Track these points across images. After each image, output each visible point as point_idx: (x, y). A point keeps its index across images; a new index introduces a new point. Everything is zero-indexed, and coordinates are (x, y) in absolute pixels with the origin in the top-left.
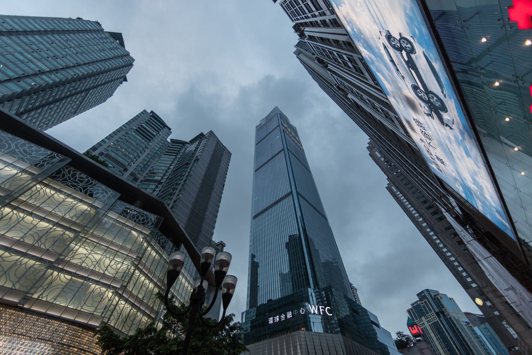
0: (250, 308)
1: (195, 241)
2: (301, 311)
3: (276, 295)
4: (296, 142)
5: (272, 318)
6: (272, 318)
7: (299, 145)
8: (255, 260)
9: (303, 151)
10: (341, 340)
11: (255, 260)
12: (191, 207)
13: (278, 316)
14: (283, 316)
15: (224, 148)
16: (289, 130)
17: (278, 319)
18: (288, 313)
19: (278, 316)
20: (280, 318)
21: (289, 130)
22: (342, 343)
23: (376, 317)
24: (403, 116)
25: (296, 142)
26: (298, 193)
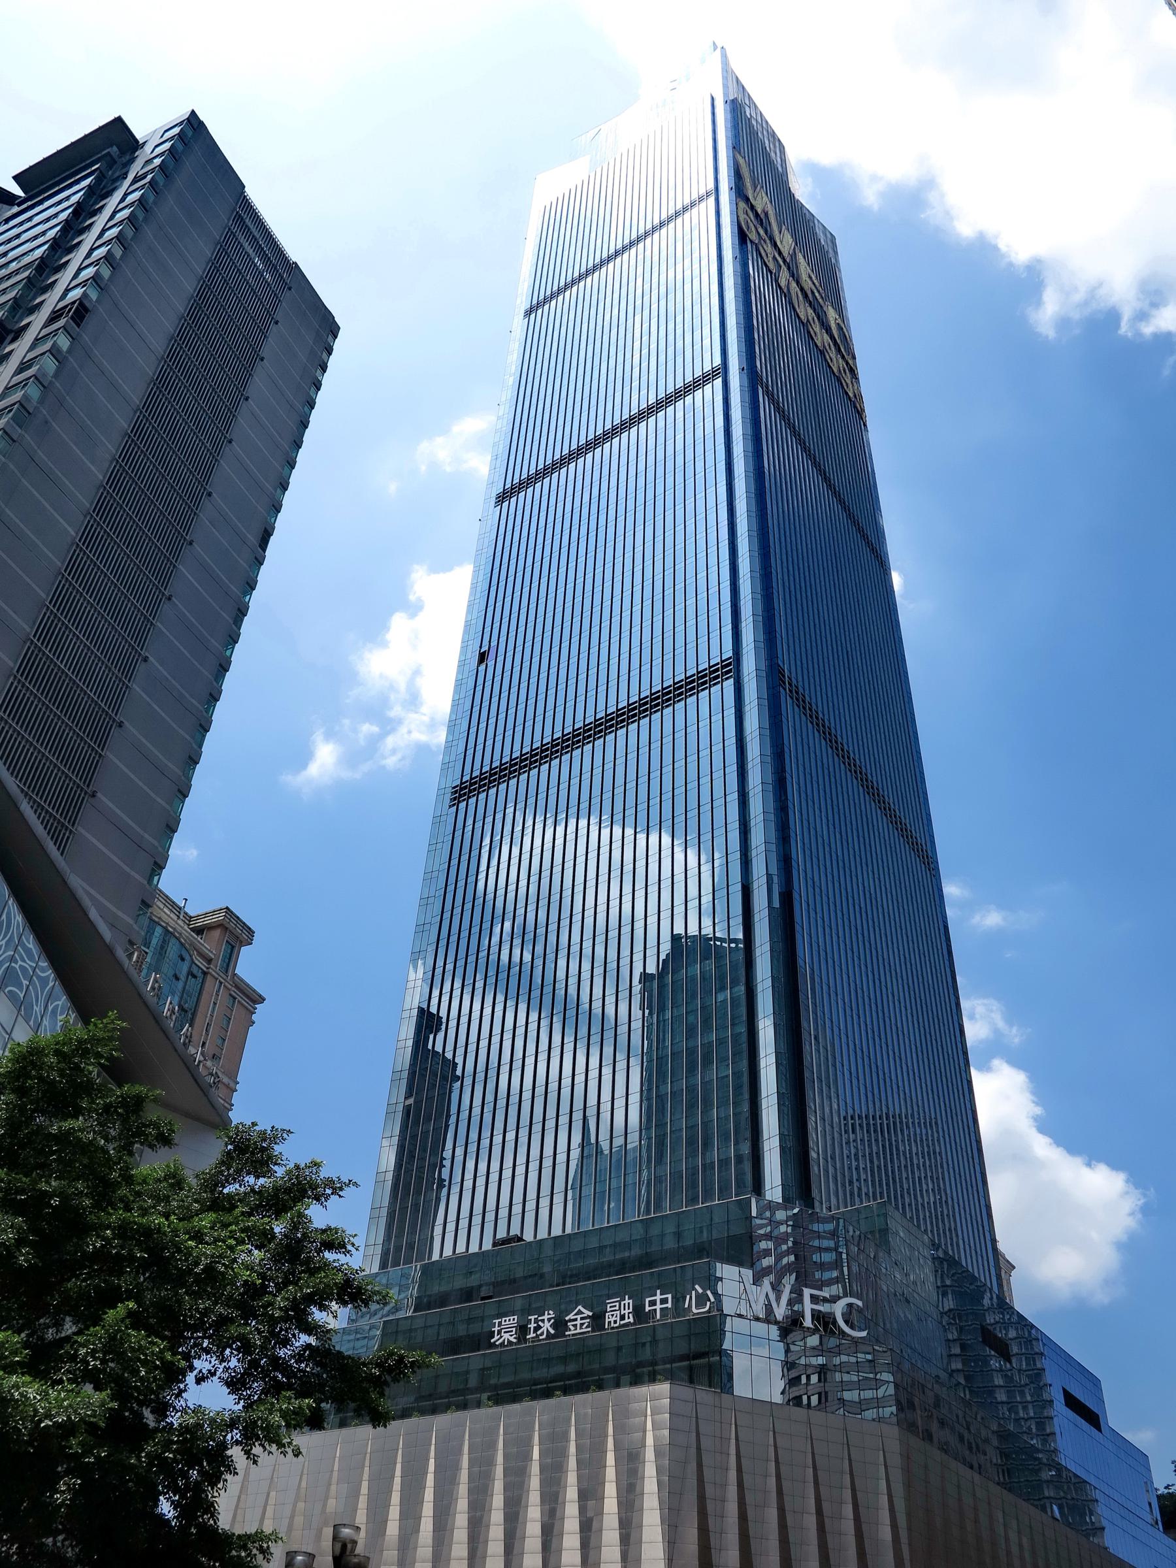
0: (383, 1265)
1: (61, 835)
2: (690, 1301)
3: (553, 1219)
4: (822, 338)
5: (511, 1321)
6: (511, 1321)
7: (837, 363)
8: (437, 1042)
9: (860, 413)
10: (894, 1446)
11: (437, 1042)
12: (26, 628)
13: (549, 1315)
14: (579, 1322)
15: (289, 275)
16: (786, 242)
17: (547, 1326)
18: (612, 1305)
19: (549, 1315)
20: (560, 1325)
21: (786, 242)
22: (896, 1460)
23: (1095, 1382)
24: (42, 302)
25: (822, 338)
26: (774, 676)
